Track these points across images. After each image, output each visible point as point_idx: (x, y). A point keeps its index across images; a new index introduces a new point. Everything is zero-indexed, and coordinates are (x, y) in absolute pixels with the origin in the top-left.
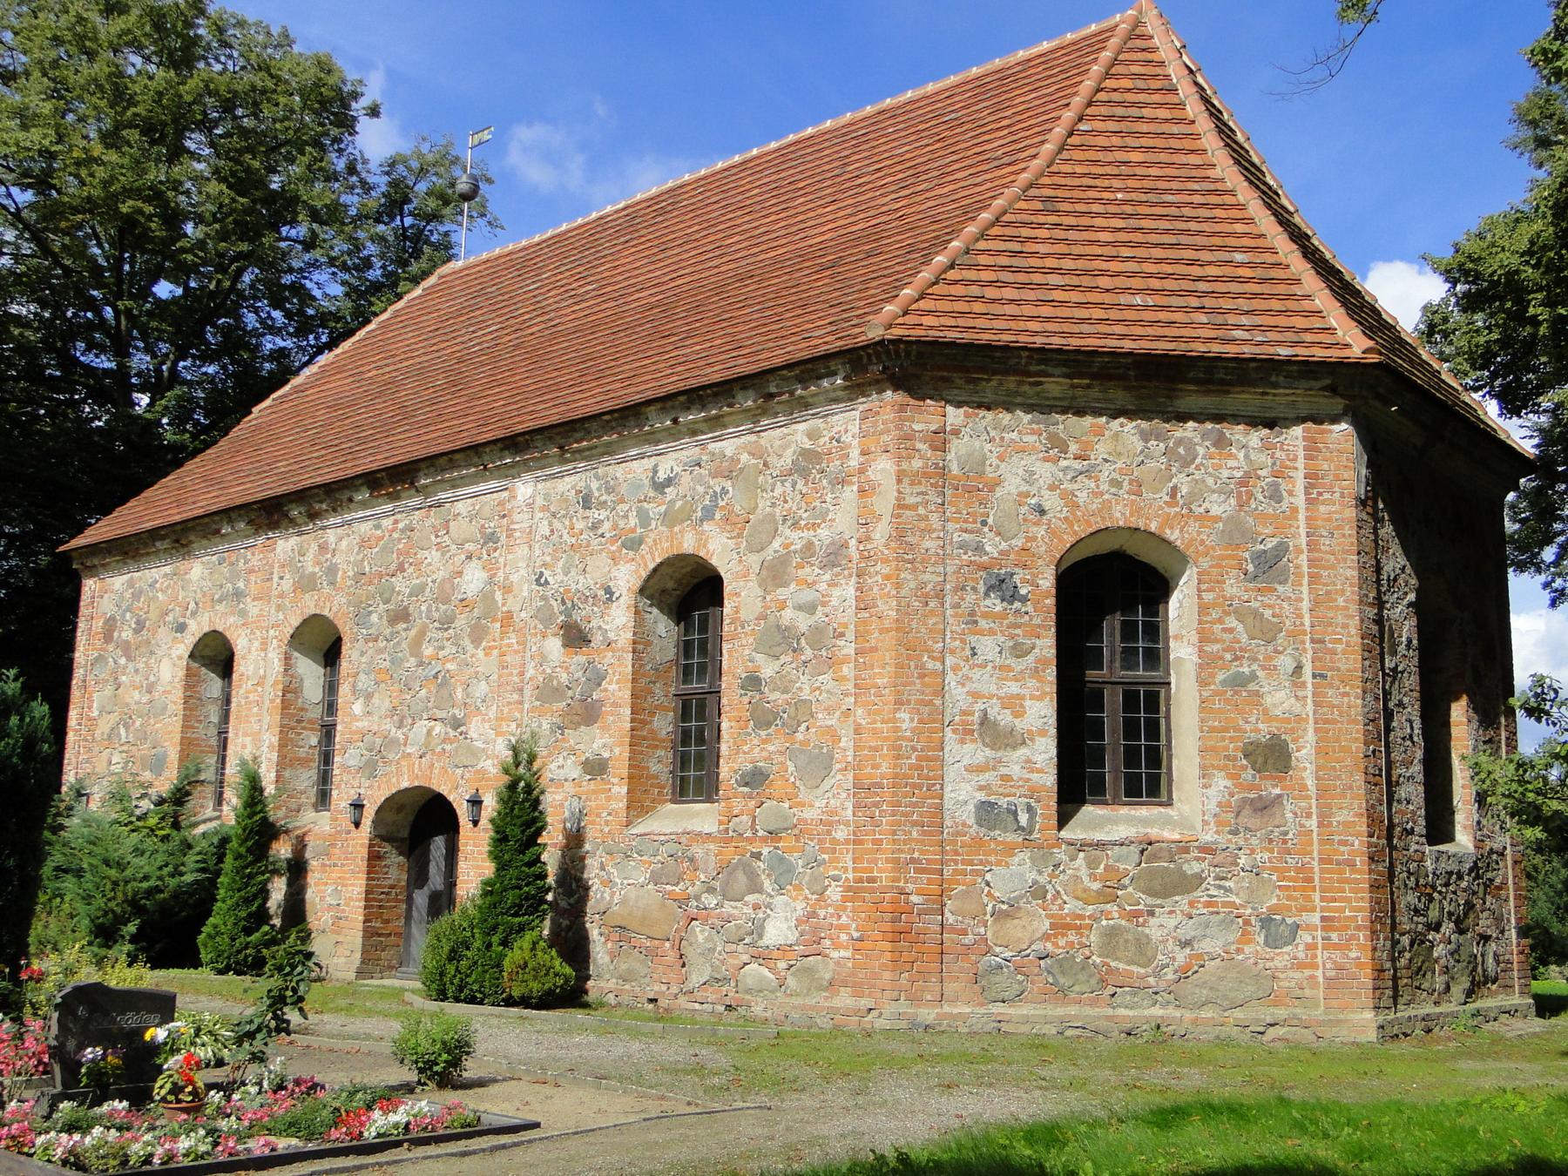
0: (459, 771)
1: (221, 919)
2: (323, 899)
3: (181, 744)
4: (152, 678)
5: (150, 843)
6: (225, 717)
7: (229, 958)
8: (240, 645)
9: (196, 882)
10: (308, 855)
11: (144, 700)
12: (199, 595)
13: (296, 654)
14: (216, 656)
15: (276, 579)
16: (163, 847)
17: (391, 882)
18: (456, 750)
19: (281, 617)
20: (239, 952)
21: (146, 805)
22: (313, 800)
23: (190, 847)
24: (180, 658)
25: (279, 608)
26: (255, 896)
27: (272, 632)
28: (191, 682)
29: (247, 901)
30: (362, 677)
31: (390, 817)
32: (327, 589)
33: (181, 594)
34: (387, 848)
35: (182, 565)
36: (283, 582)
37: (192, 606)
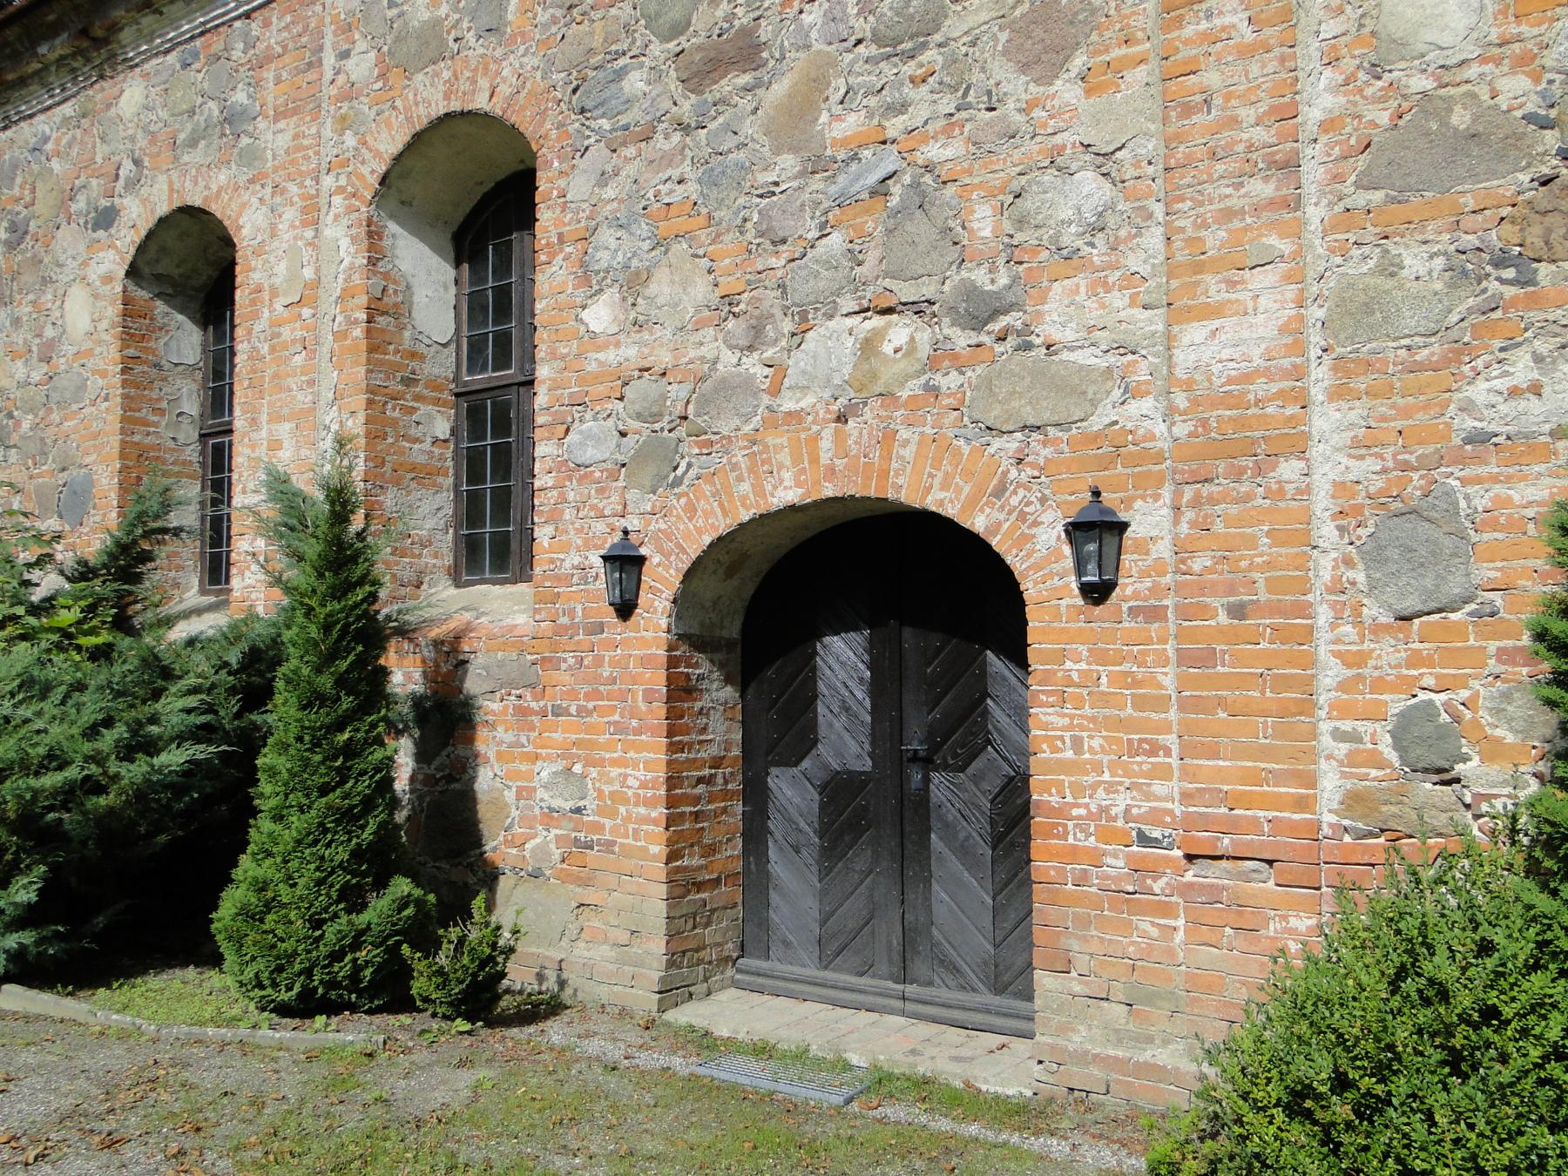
0: (1012, 444)
1: (275, 859)
2: (524, 793)
3: (123, 456)
4: (49, 332)
5: (63, 667)
6: (219, 398)
7: (308, 972)
8: (248, 224)
9: (193, 769)
10: (473, 684)
11: (36, 376)
12: (142, 141)
13: (393, 227)
14: (193, 270)
15: (329, 59)
16: (98, 675)
17: (714, 750)
18: (987, 385)
19: (350, 140)
20: (336, 956)
21: (48, 583)
22: (448, 560)
23: (167, 674)
24: (107, 279)
25: (343, 123)
26: (368, 804)
27: (328, 181)
28: (134, 328)
29: (349, 818)
30: (607, 236)
31: (711, 587)
32: (476, 48)
33: (101, 151)
34: (703, 666)
35: (98, 93)
36: (350, 64)
37: (127, 168)
